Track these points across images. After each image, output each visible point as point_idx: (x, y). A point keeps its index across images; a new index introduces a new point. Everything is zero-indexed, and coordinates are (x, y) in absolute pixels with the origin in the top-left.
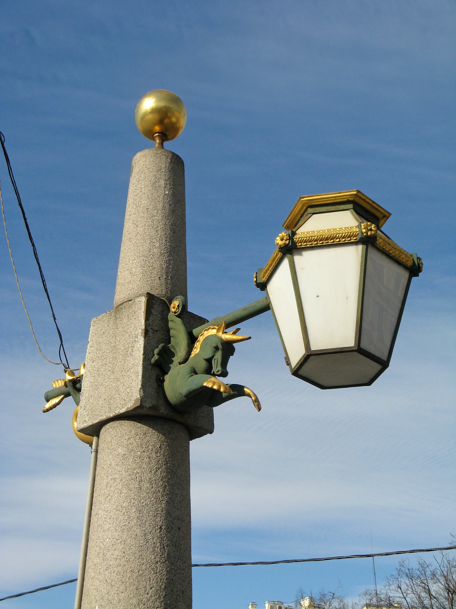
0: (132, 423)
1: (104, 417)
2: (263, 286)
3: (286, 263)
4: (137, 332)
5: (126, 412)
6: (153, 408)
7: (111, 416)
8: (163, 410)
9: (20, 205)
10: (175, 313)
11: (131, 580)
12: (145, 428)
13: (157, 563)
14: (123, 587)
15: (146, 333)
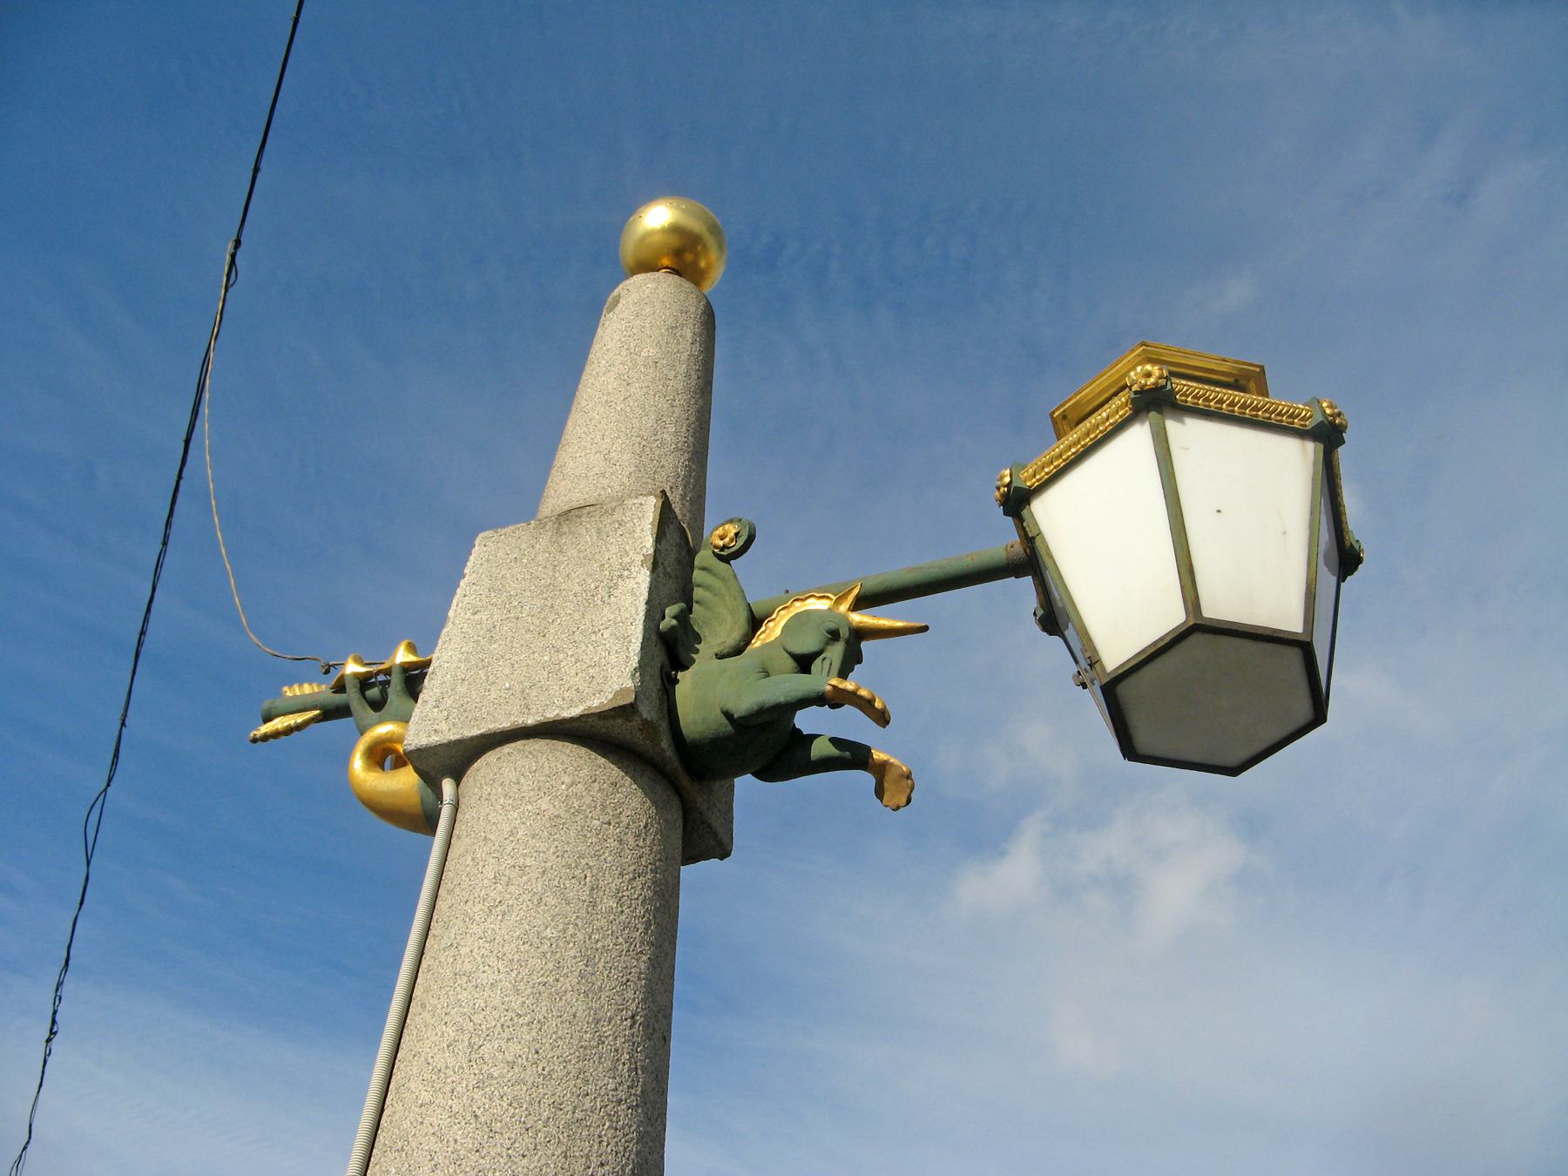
0: (583, 751)
1: (505, 724)
3: (1139, 437)
4: (627, 560)
6: (647, 726)
7: (530, 721)
9: (187, 442)
10: (724, 547)
12: (615, 772)
14: (528, 1140)
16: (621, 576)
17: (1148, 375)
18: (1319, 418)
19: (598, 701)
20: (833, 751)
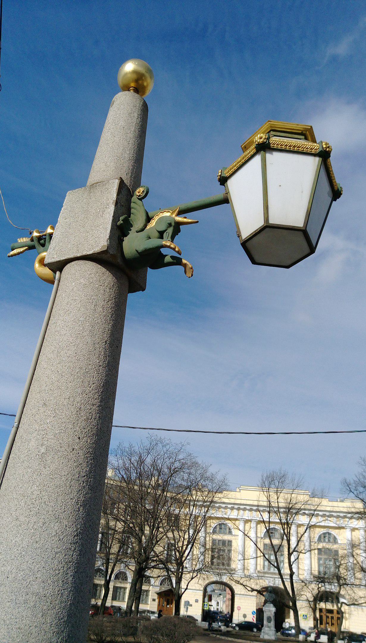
0: (94, 263)
1: (72, 256)
2: (223, 181)
3: (258, 159)
4: (108, 202)
5: (92, 254)
6: (113, 256)
7: (79, 255)
8: (119, 260)
10: (139, 196)
11: (79, 375)
12: (104, 270)
13: (100, 366)
15: (117, 203)
16: (106, 207)
17: (261, 138)
18: (321, 149)
19: (97, 249)
20: (171, 260)
